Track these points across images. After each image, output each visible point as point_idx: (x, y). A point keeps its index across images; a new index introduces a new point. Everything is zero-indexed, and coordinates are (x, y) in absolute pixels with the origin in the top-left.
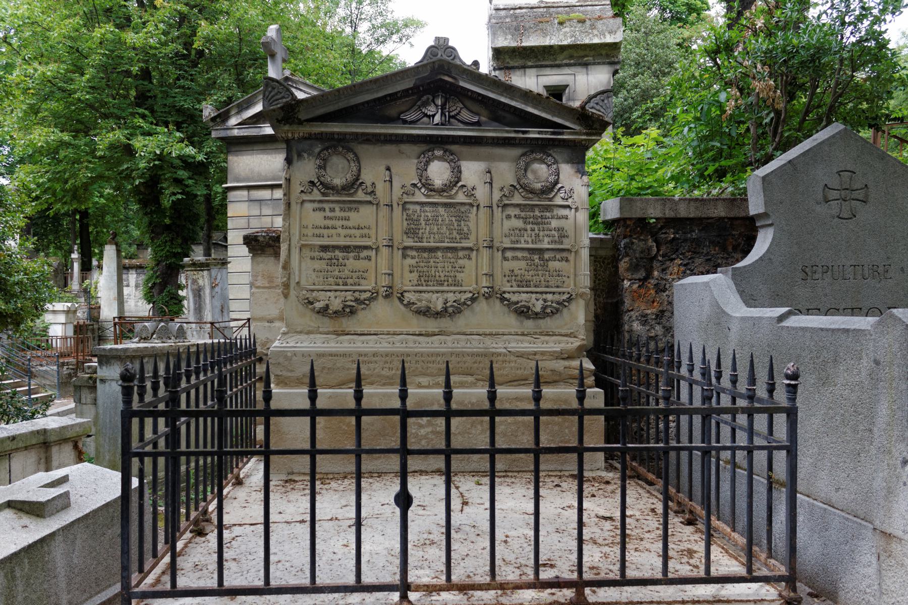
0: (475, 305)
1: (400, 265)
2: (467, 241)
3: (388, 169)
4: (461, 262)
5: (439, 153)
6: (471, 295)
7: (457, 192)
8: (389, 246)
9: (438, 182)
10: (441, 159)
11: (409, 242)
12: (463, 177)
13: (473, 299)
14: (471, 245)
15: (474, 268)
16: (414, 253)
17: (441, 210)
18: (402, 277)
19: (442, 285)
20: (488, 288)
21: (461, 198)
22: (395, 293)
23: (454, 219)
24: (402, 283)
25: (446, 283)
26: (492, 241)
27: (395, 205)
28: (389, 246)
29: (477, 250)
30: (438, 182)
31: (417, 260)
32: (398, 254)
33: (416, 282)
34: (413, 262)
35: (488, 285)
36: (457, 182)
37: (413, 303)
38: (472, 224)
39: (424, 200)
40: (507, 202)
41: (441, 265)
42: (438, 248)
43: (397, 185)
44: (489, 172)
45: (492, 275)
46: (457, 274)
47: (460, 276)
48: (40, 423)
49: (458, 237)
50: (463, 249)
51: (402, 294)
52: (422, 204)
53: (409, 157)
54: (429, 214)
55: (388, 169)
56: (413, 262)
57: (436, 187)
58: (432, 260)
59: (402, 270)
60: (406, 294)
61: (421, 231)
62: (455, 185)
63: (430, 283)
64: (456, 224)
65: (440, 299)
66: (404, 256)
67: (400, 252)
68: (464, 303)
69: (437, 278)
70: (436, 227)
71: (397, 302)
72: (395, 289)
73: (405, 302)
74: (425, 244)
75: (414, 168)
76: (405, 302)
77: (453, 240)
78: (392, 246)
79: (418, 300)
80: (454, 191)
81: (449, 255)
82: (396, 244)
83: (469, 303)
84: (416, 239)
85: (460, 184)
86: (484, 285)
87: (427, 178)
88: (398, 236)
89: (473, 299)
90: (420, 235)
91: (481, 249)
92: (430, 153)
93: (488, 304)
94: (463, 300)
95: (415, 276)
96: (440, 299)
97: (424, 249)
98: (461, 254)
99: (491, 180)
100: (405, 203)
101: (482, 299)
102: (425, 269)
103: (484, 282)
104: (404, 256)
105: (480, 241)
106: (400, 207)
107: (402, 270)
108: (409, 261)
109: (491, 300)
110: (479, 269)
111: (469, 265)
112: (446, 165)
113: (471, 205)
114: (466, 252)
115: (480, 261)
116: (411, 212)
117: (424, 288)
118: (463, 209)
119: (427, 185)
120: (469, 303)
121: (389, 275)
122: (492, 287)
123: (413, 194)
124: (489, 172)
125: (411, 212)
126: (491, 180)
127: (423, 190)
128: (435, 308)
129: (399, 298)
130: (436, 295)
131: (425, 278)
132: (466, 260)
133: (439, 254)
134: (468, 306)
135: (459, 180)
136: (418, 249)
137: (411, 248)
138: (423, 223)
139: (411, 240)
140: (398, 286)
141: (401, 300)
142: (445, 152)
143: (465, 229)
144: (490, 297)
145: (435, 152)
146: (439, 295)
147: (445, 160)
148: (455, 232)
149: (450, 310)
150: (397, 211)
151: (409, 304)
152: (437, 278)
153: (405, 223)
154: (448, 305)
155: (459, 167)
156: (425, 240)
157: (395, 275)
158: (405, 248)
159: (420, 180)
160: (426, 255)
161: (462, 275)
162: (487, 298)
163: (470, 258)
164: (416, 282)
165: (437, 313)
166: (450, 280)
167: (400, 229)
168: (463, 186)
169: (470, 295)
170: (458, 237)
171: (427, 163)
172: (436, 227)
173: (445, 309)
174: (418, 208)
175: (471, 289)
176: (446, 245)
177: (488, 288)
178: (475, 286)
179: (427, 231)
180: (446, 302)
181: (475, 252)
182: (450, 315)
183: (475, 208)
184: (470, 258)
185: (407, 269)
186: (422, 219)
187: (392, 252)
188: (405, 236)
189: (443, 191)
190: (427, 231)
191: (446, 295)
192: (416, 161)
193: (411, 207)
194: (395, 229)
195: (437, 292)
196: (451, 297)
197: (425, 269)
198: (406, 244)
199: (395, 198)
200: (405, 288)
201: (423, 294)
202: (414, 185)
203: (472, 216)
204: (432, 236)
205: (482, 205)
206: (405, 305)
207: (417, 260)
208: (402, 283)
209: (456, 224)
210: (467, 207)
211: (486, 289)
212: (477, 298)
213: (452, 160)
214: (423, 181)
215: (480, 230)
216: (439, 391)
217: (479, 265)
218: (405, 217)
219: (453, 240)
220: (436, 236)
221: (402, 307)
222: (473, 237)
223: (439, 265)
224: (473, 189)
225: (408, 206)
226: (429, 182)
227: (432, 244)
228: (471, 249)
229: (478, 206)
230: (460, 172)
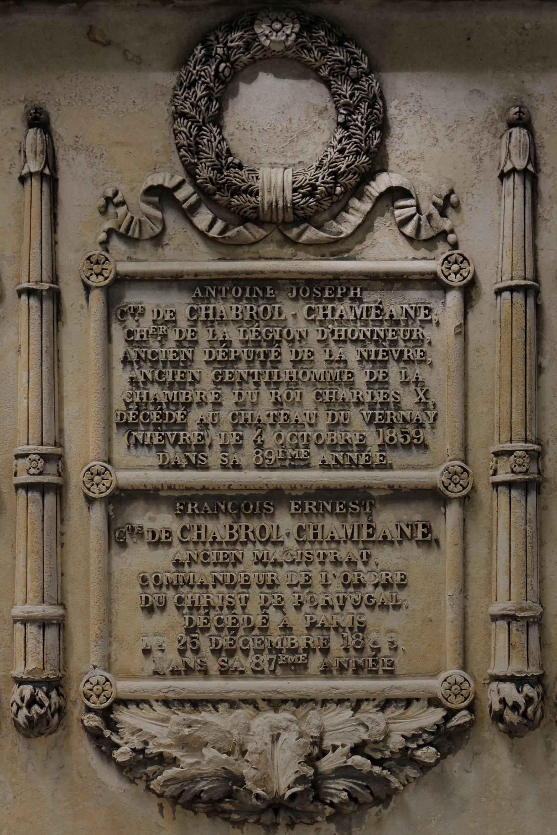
0: (455, 763)
1: (95, 577)
2: (416, 457)
3: (38, 120)
4: (387, 558)
5: (275, 34)
6: (435, 716)
7: (365, 227)
8: (42, 489)
9: (275, 181)
10: (285, 63)
11: (139, 469)
12: (396, 150)
13: (447, 738)
14: (435, 476)
15: (450, 588)
16: (164, 520)
17: (293, 313)
18: (108, 635)
19: (298, 669)
20: (519, 681)
21: (387, 251)
22: (76, 711)
23: (351, 353)
24: (108, 663)
25: (316, 661)
26: (537, 456)
27: (72, 295)
28: (42, 489)
29: (467, 501)
30: (275, 181)
31: (177, 551)
32: (88, 525)
33: (172, 658)
34: (160, 561)
35: (517, 667)
36: (369, 176)
37: (162, 760)
38: (440, 381)
39: (208, 263)
40: (126, 267)
41: (290, 573)
42: (276, 496)
43: (79, 194)
44: (523, 121)
45: (539, 621)
46: (369, 617)
47: (382, 626)
48: (328, 236)
49: (373, 439)
50: (399, 495)
51: (106, 714)
52: (201, 286)
53: (138, 62)
54: (234, 334)
55: (38, 120)
56: (160, 561)
57: (266, 198)
58: (249, 553)
59: (108, 601)
60: (126, 717)
61: (195, 415)
62: (358, 191)
63: (239, 661)
64: (361, 379)
65: (289, 738)
66: (118, 536)
67: (98, 513)
68: (405, 757)
69: (275, 637)
70: (266, 397)
71: (84, 750)
72: (77, 689)
73: (122, 755)
74: (216, 476)
75: (162, 110)
76: (122, 755)
77: (347, 454)
78: (59, 490)
79: (184, 743)
80: (352, 220)
81: (332, 525)
82: (76, 478)
83: (427, 754)
84: (172, 453)
85: (381, 183)
86: (500, 667)
87: (225, 160)
88: (83, 444)
89: (447, 738)
90: (192, 433)
91: (485, 492)
92: (236, 38)
93: (518, 755)
94: (396, 742)
95: (168, 626)
96: (289, 738)
97: (211, 501)
98: (387, 520)
99: (534, 159)
100: (122, 281)
101: (489, 732)
102: (217, 595)
103: (501, 655)
104: (118, 536)
105: (481, 459)
106: (97, 297)
107: (108, 601)
108: (140, 559)
109: (534, 739)
110: (475, 589)
111: (428, 572)
112: (313, 93)
113: (433, 283)
114: (412, 513)
115: (478, 549)
116: (146, 323)
117: (215, 686)
118: (396, 303)
119: (218, 188)
120: (427, 754)
121: (43, 624)
122: (537, 681)
123: (158, 240)
124: (523, 121)
125: (146, 323)
126: (534, 159)
127: (203, 218)
128: (264, 781)
129: (95, 736)
130: (269, 717)
131: (215, 639)
132: (411, 550)
133: (285, 522)
134: (424, 767)
135: (378, 163)
136: (184, 501)
137: (150, 495)
138: (207, 375)
139: (151, 458)
140: (86, 669)
141: (103, 744)
142: (308, 27)
143: (409, 400)
144: (529, 723)
145: (262, 29)
146: (283, 717)
147: (309, 71)
148: (357, 418)
149: (338, 789)
150: (84, 319)
151: (141, 766)
152: (275, 637)
153: (121, 377)
154: (327, 764)
155: (377, 102)
156: (214, 456)
157: (75, 623)
158: (121, 498)
159: (191, 171)
160: (219, 527)
161: (392, 619)
162: (512, 732)
163: (429, 541)
164: (172, 658)
165: (276, 805)
166: (336, 643)
167: (94, 405)
168: (396, 193)
169: (433, 717)
170: (373, 439)
171: (223, 89)
172: (266, 397)
173: (314, 786)
174: (180, 303)
175: (435, 686)
176: (314, 476)
177: (519, 681)
178: (454, 672)
179: (225, 414)
180: (316, 751)
181: (453, 512)
182: (338, 814)
183: (454, 299)
184: (429, 541)
185: (130, 596)
186: (200, 356)
187: (61, 516)
188: (120, 441)
189: (302, 217)
190: (225, 414)
191: (314, 718)
192: (170, 80)
193: (149, 300)
194: (70, 410)
195: (276, 703)
196: (341, 727)
197: (217, 595)
198: (125, 477)
199: (71, 262)
200: (124, 687)
201: (206, 715)
202: (160, 195)
203: (442, 337)
204: (250, 435)
205: (487, 286)
206: (121, 767)
207: (177, 551)
208: (108, 663)
209: (361, 379)
210: (417, 296)
211: (509, 690)
212: (464, 730)
213: (340, 71)
214: (204, 173)
215: (478, 405)
216: (273, 233)
217: (476, 571)
218: (119, 347)
219: (347, 454)
220: (270, 438)
221: (110, 778)
222: (443, 439)
223: (282, 574)
224: (447, 205)
225: (132, 297)
226: (232, 176)
227: (250, 476)
228: (434, 496)
229: (469, 290)
230: (383, 127)
